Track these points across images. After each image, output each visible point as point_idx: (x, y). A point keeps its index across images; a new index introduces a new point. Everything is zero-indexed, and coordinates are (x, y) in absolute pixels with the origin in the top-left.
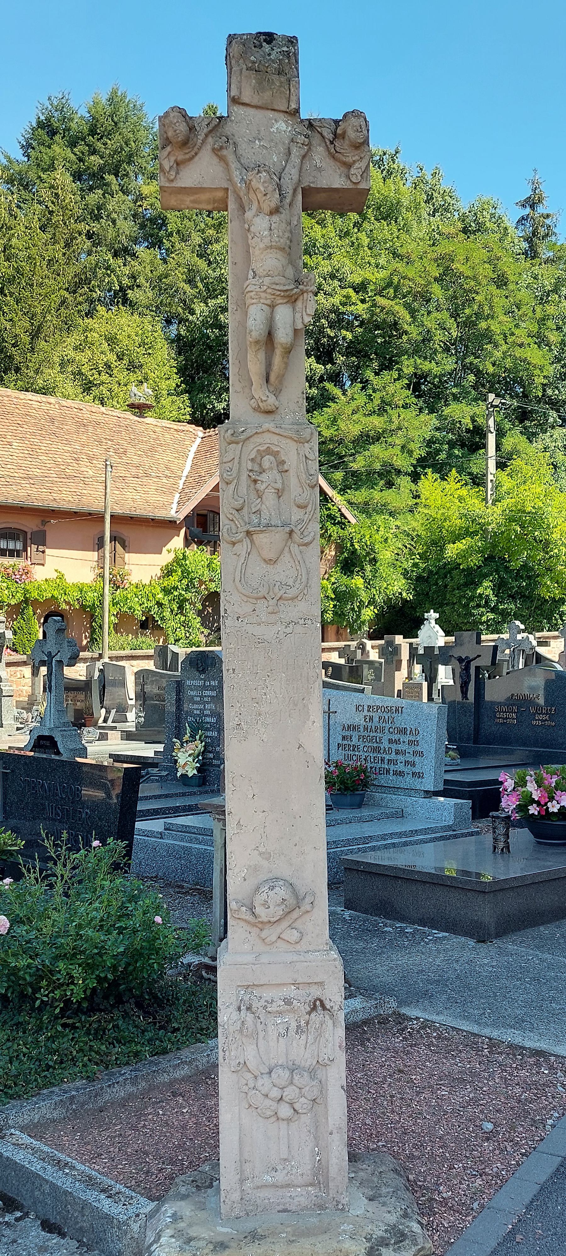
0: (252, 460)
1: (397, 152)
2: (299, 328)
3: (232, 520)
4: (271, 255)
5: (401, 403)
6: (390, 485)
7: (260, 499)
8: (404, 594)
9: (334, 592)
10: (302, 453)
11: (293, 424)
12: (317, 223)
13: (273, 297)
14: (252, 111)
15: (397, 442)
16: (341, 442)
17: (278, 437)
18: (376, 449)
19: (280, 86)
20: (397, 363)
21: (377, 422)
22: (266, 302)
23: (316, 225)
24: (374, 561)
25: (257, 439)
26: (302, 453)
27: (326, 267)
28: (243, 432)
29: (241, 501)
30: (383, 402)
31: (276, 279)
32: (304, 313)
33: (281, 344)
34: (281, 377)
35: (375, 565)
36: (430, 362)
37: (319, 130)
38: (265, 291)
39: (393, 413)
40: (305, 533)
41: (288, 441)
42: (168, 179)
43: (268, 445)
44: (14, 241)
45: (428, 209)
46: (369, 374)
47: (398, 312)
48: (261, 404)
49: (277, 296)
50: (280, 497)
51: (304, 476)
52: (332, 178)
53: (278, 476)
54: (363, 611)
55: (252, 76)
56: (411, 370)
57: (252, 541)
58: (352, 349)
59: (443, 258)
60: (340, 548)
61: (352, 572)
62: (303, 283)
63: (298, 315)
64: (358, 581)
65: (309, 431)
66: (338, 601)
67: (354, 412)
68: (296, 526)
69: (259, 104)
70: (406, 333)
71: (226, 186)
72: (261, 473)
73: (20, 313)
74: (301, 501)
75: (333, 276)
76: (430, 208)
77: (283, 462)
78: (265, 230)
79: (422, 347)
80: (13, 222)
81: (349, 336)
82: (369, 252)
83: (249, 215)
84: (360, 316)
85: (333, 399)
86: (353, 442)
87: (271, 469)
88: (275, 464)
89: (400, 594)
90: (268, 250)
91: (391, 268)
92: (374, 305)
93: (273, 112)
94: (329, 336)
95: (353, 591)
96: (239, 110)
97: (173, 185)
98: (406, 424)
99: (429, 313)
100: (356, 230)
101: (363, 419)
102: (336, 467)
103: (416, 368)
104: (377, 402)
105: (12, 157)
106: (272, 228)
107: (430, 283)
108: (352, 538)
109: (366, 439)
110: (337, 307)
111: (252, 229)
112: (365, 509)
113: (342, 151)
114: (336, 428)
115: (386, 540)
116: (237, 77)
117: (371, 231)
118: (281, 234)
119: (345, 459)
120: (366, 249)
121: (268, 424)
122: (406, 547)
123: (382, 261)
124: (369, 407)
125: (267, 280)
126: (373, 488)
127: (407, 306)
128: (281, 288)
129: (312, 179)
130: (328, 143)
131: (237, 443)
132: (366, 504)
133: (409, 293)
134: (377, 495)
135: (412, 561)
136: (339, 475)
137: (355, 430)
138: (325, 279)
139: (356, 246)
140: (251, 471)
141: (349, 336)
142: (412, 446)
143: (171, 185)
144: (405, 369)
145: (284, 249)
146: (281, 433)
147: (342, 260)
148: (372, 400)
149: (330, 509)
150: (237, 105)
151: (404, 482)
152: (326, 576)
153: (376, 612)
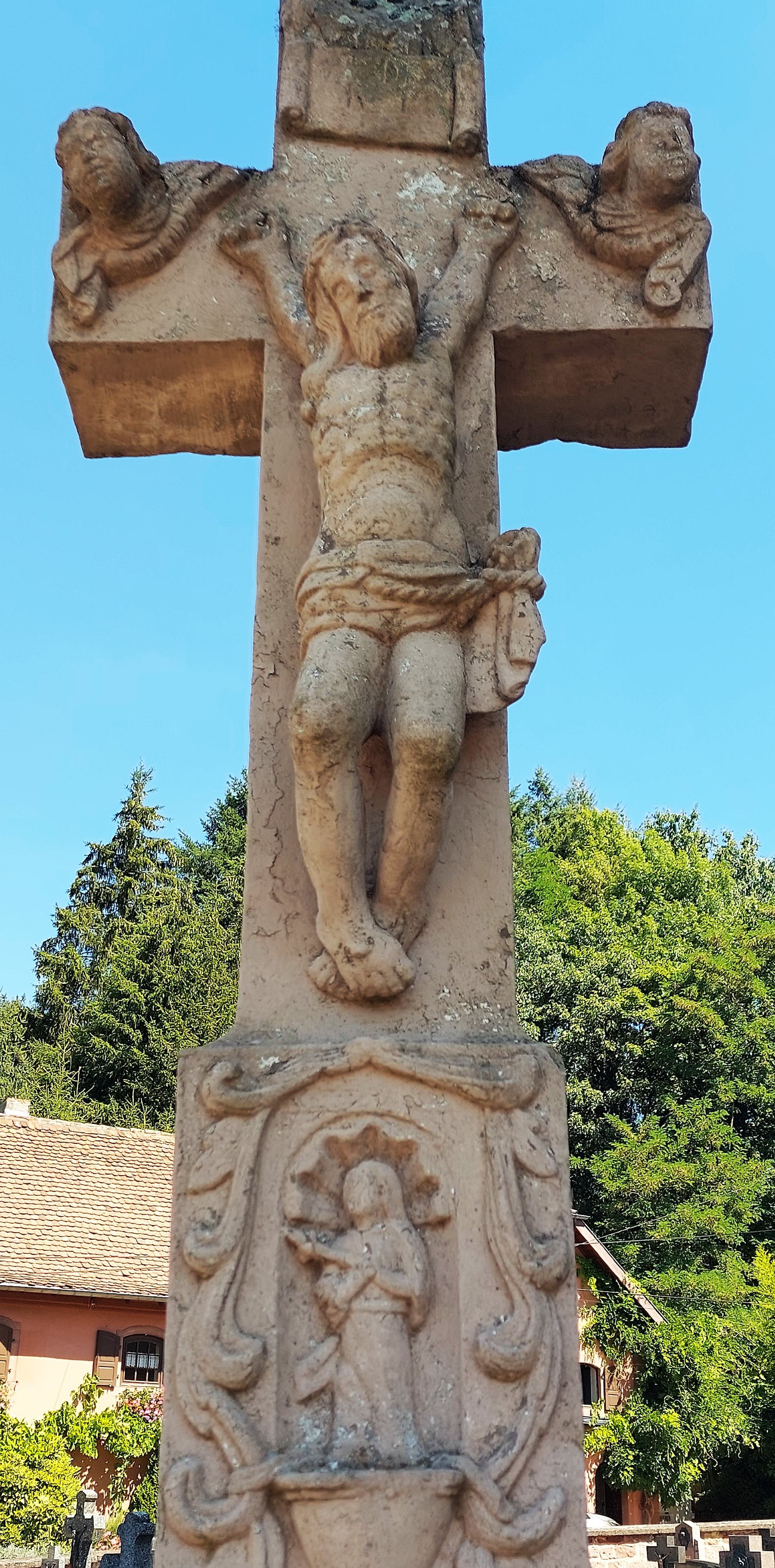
0: (307, 1180)
1: (693, 817)
2: (484, 709)
3: (209, 1437)
4: (380, 477)
5: (719, 1143)
6: (711, 1263)
7: (332, 1342)
8: (746, 1439)
9: (635, 1433)
10: (502, 1147)
11: (467, 1039)
12: (587, 905)
13: (390, 604)
14: (341, 154)
15: (718, 1200)
16: (633, 1198)
17: (408, 1088)
18: (685, 1209)
19: (426, 81)
20: (710, 1087)
21: (686, 1171)
22: (363, 621)
23: (585, 908)
24: (694, 1383)
25: (328, 1099)
26: (502, 1147)
27: (600, 960)
28: (274, 1069)
29: (249, 1351)
30: (692, 1141)
31: (402, 547)
32: (502, 658)
33: (415, 746)
34: (424, 873)
35: (696, 1390)
36: (758, 1085)
37: (545, 184)
38: (358, 585)
39: (710, 1158)
40: (524, 1496)
41: (450, 1102)
42: (75, 318)
43: (368, 1120)
44: (186, 940)
45: (740, 887)
46: (670, 1103)
47: (706, 1017)
48: (346, 970)
49: (406, 599)
50: (413, 1331)
51: (513, 1242)
52: (594, 305)
53: (408, 1246)
54: (682, 1467)
55: (344, 60)
56: (732, 1096)
57: (289, 1536)
58: (645, 1067)
59: (765, 945)
60: (640, 1362)
61: (661, 1401)
62: (496, 561)
63: (480, 669)
64: (671, 1417)
65: (526, 1063)
66: (641, 1450)
67: (651, 1156)
68: (481, 1464)
69: (365, 130)
70: (720, 1045)
71: (256, 335)
72: (340, 1232)
73: (187, 1030)
74: (501, 1351)
75: (610, 971)
76: (742, 885)
77: (429, 1187)
78: (363, 402)
79: (743, 1065)
80: (185, 916)
81: (638, 1050)
82: (659, 941)
83: (312, 373)
84: (650, 1023)
85: (619, 1138)
86: (652, 1200)
87: (379, 1213)
88: (397, 1193)
89: (740, 1438)
90: (374, 462)
91: (692, 960)
92: (672, 1008)
93: (405, 154)
94: (609, 1052)
95: (664, 1432)
96: (308, 153)
97: (93, 337)
98: (728, 1174)
99: (751, 1018)
100: (639, 913)
101: (665, 1166)
102: (625, 1236)
103: (738, 1095)
104: (684, 1141)
105: (193, 840)
106: (388, 395)
107: (750, 977)
108: (657, 1346)
109: (669, 1196)
110: (619, 1013)
111: (322, 411)
112: (674, 1300)
113: (619, 223)
114: (625, 1178)
115: (710, 1351)
116: (298, 62)
117: (660, 914)
118: (418, 413)
119: (641, 1225)
120: (655, 936)
121: (369, 1038)
122: (742, 1361)
123: (679, 951)
124: (673, 1149)
125: (367, 551)
126: (685, 1268)
127: (719, 1009)
128: (420, 571)
129: (525, 310)
130: (573, 212)
131: (246, 1113)
132: (677, 1292)
133: (720, 991)
134: (693, 1279)
135: (754, 1384)
136: (632, 1249)
137: (654, 1182)
138: (600, 976)
139: (641, 933)
140: (299, 1222)
141: (638, 1050)
142: (740, 1206)
143: (87, 339)
144: (721, 1096)
145: (428, 455)
146: (421, 1072)
147: (621, 949)
148: (676, 1139)
149: (621, 1301)
150: (299, 142)
151: (732, 1259)
152: (621, 1408)
153: (703, 1469)
